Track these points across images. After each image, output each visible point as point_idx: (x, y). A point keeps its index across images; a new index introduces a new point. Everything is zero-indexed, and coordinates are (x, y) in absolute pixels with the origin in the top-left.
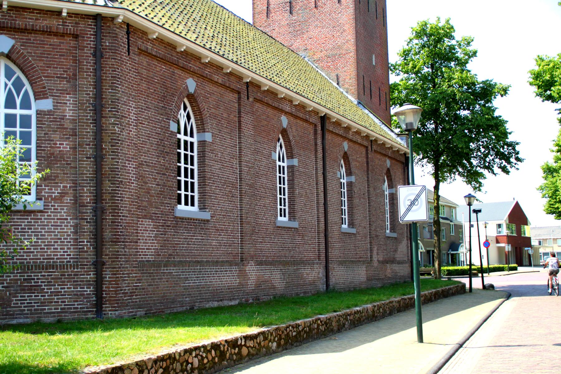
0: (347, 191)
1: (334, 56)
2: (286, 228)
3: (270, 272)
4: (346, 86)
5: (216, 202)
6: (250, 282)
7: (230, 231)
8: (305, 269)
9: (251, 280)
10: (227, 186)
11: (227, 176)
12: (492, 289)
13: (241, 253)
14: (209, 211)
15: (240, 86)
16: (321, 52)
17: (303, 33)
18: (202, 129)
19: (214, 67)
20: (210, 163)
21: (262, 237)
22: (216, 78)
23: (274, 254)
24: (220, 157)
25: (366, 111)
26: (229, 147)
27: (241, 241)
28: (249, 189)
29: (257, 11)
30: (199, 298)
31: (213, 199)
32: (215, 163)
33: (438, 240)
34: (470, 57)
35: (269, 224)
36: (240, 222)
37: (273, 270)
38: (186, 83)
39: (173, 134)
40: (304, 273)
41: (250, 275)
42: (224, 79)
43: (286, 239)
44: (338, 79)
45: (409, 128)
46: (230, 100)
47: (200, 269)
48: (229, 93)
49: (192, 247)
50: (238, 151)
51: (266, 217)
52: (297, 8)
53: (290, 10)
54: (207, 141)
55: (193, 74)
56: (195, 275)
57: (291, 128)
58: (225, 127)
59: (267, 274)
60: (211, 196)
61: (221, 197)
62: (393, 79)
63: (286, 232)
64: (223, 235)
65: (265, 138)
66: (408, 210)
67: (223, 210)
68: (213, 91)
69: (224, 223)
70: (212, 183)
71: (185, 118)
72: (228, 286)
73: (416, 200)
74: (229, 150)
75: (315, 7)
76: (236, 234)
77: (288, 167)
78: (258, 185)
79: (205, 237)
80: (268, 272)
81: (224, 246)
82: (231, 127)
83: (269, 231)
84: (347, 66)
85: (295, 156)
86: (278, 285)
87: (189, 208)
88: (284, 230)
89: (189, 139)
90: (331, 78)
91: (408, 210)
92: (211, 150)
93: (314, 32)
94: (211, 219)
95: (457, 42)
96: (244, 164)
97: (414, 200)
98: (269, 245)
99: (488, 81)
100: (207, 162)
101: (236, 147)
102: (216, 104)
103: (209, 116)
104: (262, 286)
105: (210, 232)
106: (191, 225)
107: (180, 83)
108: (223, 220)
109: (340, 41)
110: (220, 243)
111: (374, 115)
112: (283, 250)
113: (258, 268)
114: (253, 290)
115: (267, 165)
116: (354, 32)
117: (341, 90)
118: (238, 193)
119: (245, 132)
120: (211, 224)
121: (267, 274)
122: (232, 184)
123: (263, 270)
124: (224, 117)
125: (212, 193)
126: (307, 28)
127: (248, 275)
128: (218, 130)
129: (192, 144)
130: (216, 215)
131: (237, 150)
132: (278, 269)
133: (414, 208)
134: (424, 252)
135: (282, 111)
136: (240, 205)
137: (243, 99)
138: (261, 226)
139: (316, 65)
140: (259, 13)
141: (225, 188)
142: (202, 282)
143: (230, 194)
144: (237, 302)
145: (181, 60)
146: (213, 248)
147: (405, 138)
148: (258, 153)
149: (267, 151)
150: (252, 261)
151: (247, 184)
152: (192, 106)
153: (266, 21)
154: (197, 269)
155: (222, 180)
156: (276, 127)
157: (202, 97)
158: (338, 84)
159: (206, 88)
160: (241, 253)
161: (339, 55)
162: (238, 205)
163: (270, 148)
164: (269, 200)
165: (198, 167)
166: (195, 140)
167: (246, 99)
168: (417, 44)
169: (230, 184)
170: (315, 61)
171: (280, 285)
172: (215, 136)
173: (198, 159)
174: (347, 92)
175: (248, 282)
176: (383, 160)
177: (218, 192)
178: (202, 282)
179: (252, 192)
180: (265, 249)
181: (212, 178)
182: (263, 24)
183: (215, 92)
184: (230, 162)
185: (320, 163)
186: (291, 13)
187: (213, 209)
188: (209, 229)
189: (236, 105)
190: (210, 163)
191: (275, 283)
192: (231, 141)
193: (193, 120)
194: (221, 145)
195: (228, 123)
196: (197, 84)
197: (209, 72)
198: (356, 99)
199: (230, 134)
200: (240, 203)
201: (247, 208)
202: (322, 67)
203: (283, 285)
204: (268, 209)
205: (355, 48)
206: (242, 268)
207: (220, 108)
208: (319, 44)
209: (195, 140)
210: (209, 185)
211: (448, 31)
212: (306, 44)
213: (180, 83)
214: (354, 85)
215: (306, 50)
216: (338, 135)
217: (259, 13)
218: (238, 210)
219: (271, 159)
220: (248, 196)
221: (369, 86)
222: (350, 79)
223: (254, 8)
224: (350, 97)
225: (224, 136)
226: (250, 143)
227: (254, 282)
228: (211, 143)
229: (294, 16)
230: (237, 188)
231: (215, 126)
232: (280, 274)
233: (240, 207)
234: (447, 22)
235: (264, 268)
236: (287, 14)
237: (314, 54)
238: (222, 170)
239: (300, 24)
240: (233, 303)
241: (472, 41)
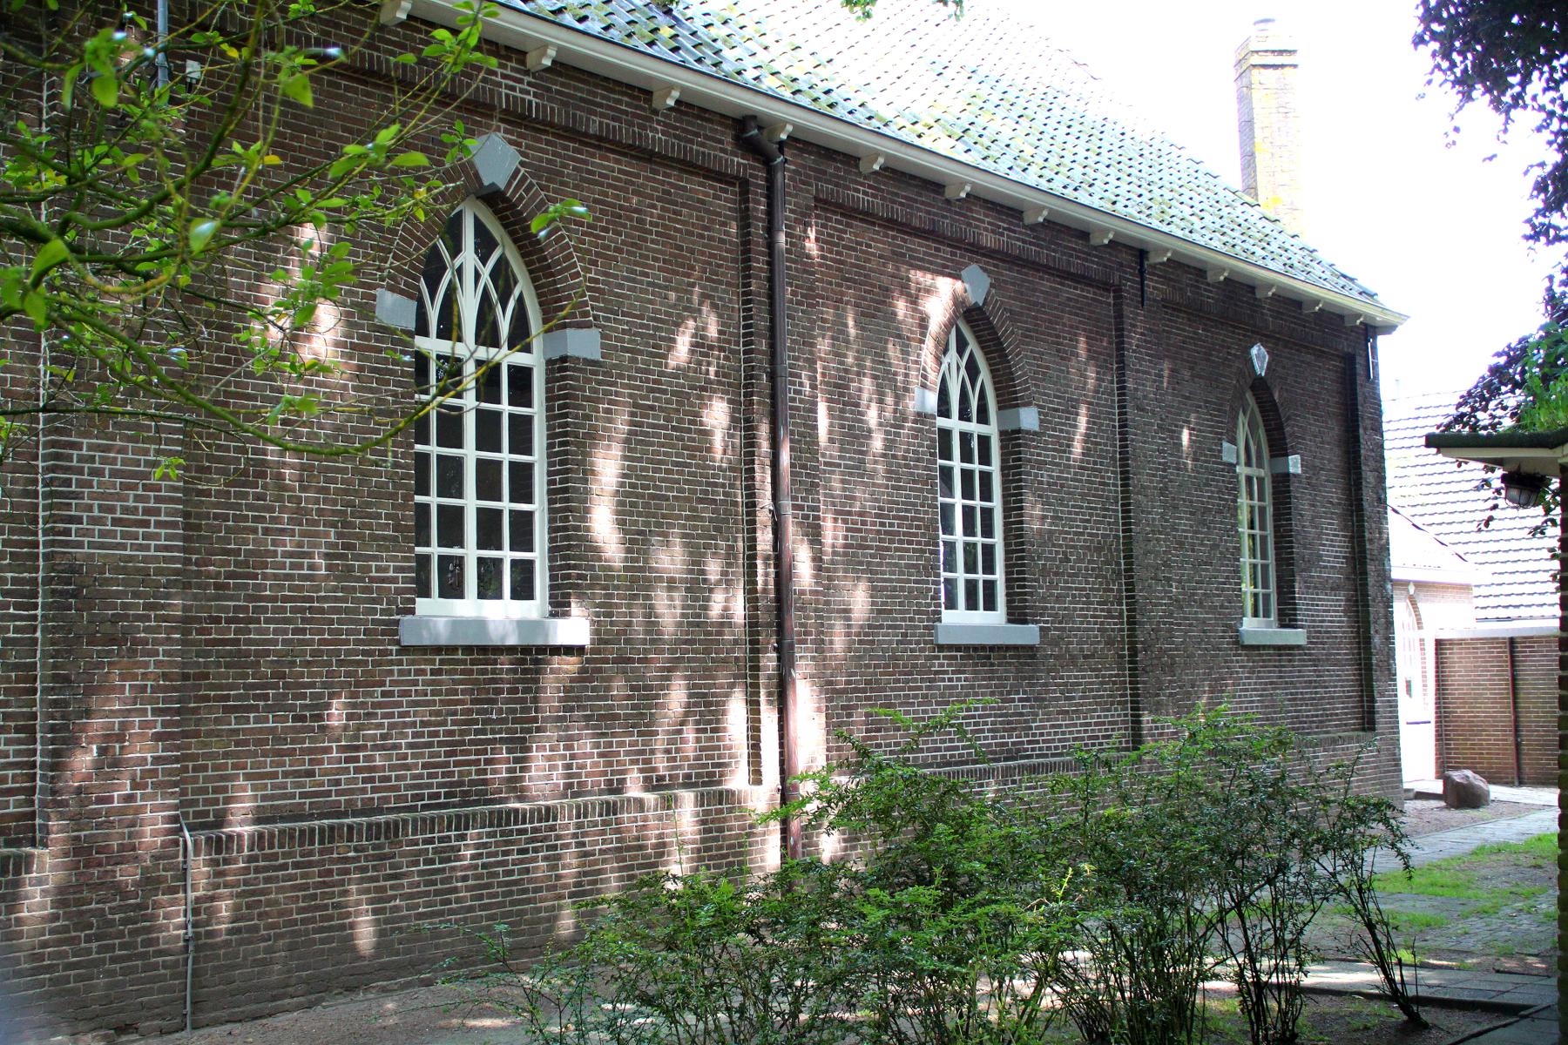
18: (1009, 400)
39: (399, 339)
71: (963, 372)
87: (980, 617)
89: (974, 427)
129: (984, 441)
166: (533, 360)
209: (992, 430)
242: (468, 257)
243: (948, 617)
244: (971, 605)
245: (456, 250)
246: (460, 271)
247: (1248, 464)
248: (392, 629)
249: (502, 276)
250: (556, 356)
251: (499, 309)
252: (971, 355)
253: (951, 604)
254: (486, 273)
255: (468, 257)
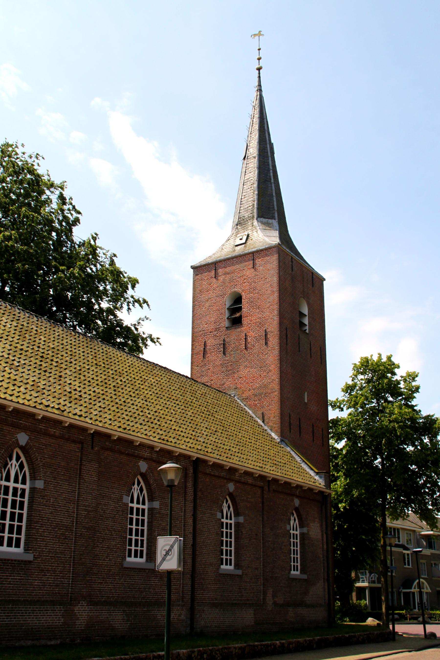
0: (235, 531)
1: (260, 394)
2: (138, 569)
3: (108, 613)
4: (271, 424)
5: (43, 544)
6: (79, 622)
7: (59, 571)
8: (160, 610)
9: (80, 620)
10: (59, 529)
11: (59, 519)
12: (433, 638)
13: (71, 594)
14: (33, 553)
15: (83, 437)
16: (249, 390)
17: (234, 373)
19: (51, 421)
20: (39, 507)
21: (102, 578)
22: (52, 431)
23: (118, 595)
24: (53, 502)
25: (288, 449)
26: (65, 493)
27: (72, 581)
28: (85, 532)
29: (195, 351)
30: (7, 636)
31: (39, 541)
32: (45, 508)
33: (384, 581)
34: (413, 392)
35: (114, 565)
36: (73, 563)
37: (112, 610)
38: (16, 437)
40: (158, 614)
41: (80, 615)
42: (63, 432)
43: (137, 580)
44: (263, 417)
45: (170, 484)
46: (71, 450)
47: (12, 608)
48: (69, 443)
49: (6, 587)
50: (77, 496)
51: (110, 559)
52: (230, 349)
53: (224, 351)
54: (37, 488)
55: (25, 429)
56: (4, 613)
57: (151, 472)
58: (62, 475)
59: (103, 615)
60: (37, 538)
61: (50, 540)
62: (333, 414)
63: (137, 573)
64: (49, 575)
65: (115, 483)
66: (164, 559)
67: (51, 552)
68: (49, 442)
69: (52, 563)
70: (39, 526)
71: (139, 491)
72: (47, 625)
73: (170, 550)
74: (65, 495)
75: (245, 348)
76: (67, 574)
77: (149, 509)
78: (102, 527)
79: (24, 577)
80: (105, 613)
81: (49, 586)
82: (70, 474)
83: (112, 572)
84: (272, 405)
85: (157, 498)
86: (118, 626)
88: (134, 571)
90: (258, 416)
91: (164, 559)
92: (41, 496)
93: (244, 372)
94: (34, 560)
95: (402, 377)
96: (82, 509)
97: (169, 550)
98: (111, 585)
99: (429, 416)
100: (35, 507)
101: (75, 493)
102: (52, 454)
103: (42, 466)
104: (95, 627)
105: (32, 572)
106: (8, 566)
107: (8, 437)
108: (51, 561)
109: (265, 381)
110: (45, 583)
111: (295, 453)
112: (132, 591)
113: (91, 608)
114: (82, 630)
115: (115, 508)
116: (279, 372)
117: (266, 428)
118: (73, 535)
119: (86, 478)
120: (34, 565)
121: (103, 615)
122: (66, 527)
123: (99, 610)
124: (61, 465)
125: (38, 536)
126: (238, 368)
127: (77, 615)
128: (53, 477)
129: (143, 510)
130: (41, 556)
131: (76, 495)
132: (120, 610)
133: (168, 557)
134: (430, 593)
135: (140, 458)
136: (74, 547)
137: (86, 448)
138: (102, 567)
139: (245, 403)
140: (197, 354)
141: (57, 531)
142: (13, 621)
143: (63, 536)
144: (59, 642)
145: (10, 418)
146: (34, 588)
147: (323, 476)
148: (103, 498)
149: (116, 495)
150: (84, 601)
151: (84, 527)
152: (26, 457)
153: (202, 361)
154: (8, 608)
155: (53, 523)
156: (131, 472)
157: (35, 448)
158: (263, 422)
159: (40, 440)
160: (71, 594)
161: (265, 394)
162: (72, 546)
163: (121, 492)
164: (116, 542)
165: (28, 512)
167: (90, 448)
168: (362, 379)
169: (63, 527)
170: (243, 399)
171: (121, 626)
172: (48, 483)
173: (28, 504)
174: (271, 430)
175: (76, 622)
176: (288, 499)
177: (47, 534)
178: (13, 621)
179: (90, 534)
180: (106, 590)
181: (40, 522)
182: (200, 364)
183: (52, 443)
184: (67, 507)
185: (190, 506)
186: (224, 353)
187: (38, 551)
188: (31, 570)
189: (79, 454)
190: (39, 507)
191: (114, 624)
192: (69, 487)
193: (26, 468)
194: (55, 491)
195: (65, 471)
196: (30, 438)
197: (44, 426)
198: (279, 437)
199: (69, 480)
200: (74, 544)
201: (82, 549)
202: (249, 405)
203: (126, 626)
204: (113, 550)
205: (279, 387)
206: (69, 608)
207: (57, 458)
208: (248, 383)
210: (35, 528)
211: (389, 367)
212: (236, 383)
213: (8, 437)
214: (278, 423)
215: (236, 388)
216: (219, 477)
217: (197, 354)
218: (72, 551)
219: (122, 503)
220: (84, 538)
221: (298, 423)
222: (274, 417)
223: (192, 349)
224: (273, 435)
225: (59, 483)
226: (91, 488)
227: (84, 622)
228: (42, 489)
229: (227, 357)
230: (73, 530)
231: (49, 474)
232: (123, 615)
233: (74, 549)
234: (389, 358)
235: (100, 608)
236: (221, 355)
237: (243, 393)
238: (54, 514)
239: (231, 364)
240: (53, 643)
241: (417, 376)
242: (14, 461)
243: (128, 559)
244: (226, 564)
245: (11, 459)
246: (11, 465)
247: (293, 530)
248: (122, 564)
249: (21, 466)
250: (32, 487)
251: (3, 470)
252: (141, 486)
253: (130, 556)
254: (17, 465)
255: (14, 461)
